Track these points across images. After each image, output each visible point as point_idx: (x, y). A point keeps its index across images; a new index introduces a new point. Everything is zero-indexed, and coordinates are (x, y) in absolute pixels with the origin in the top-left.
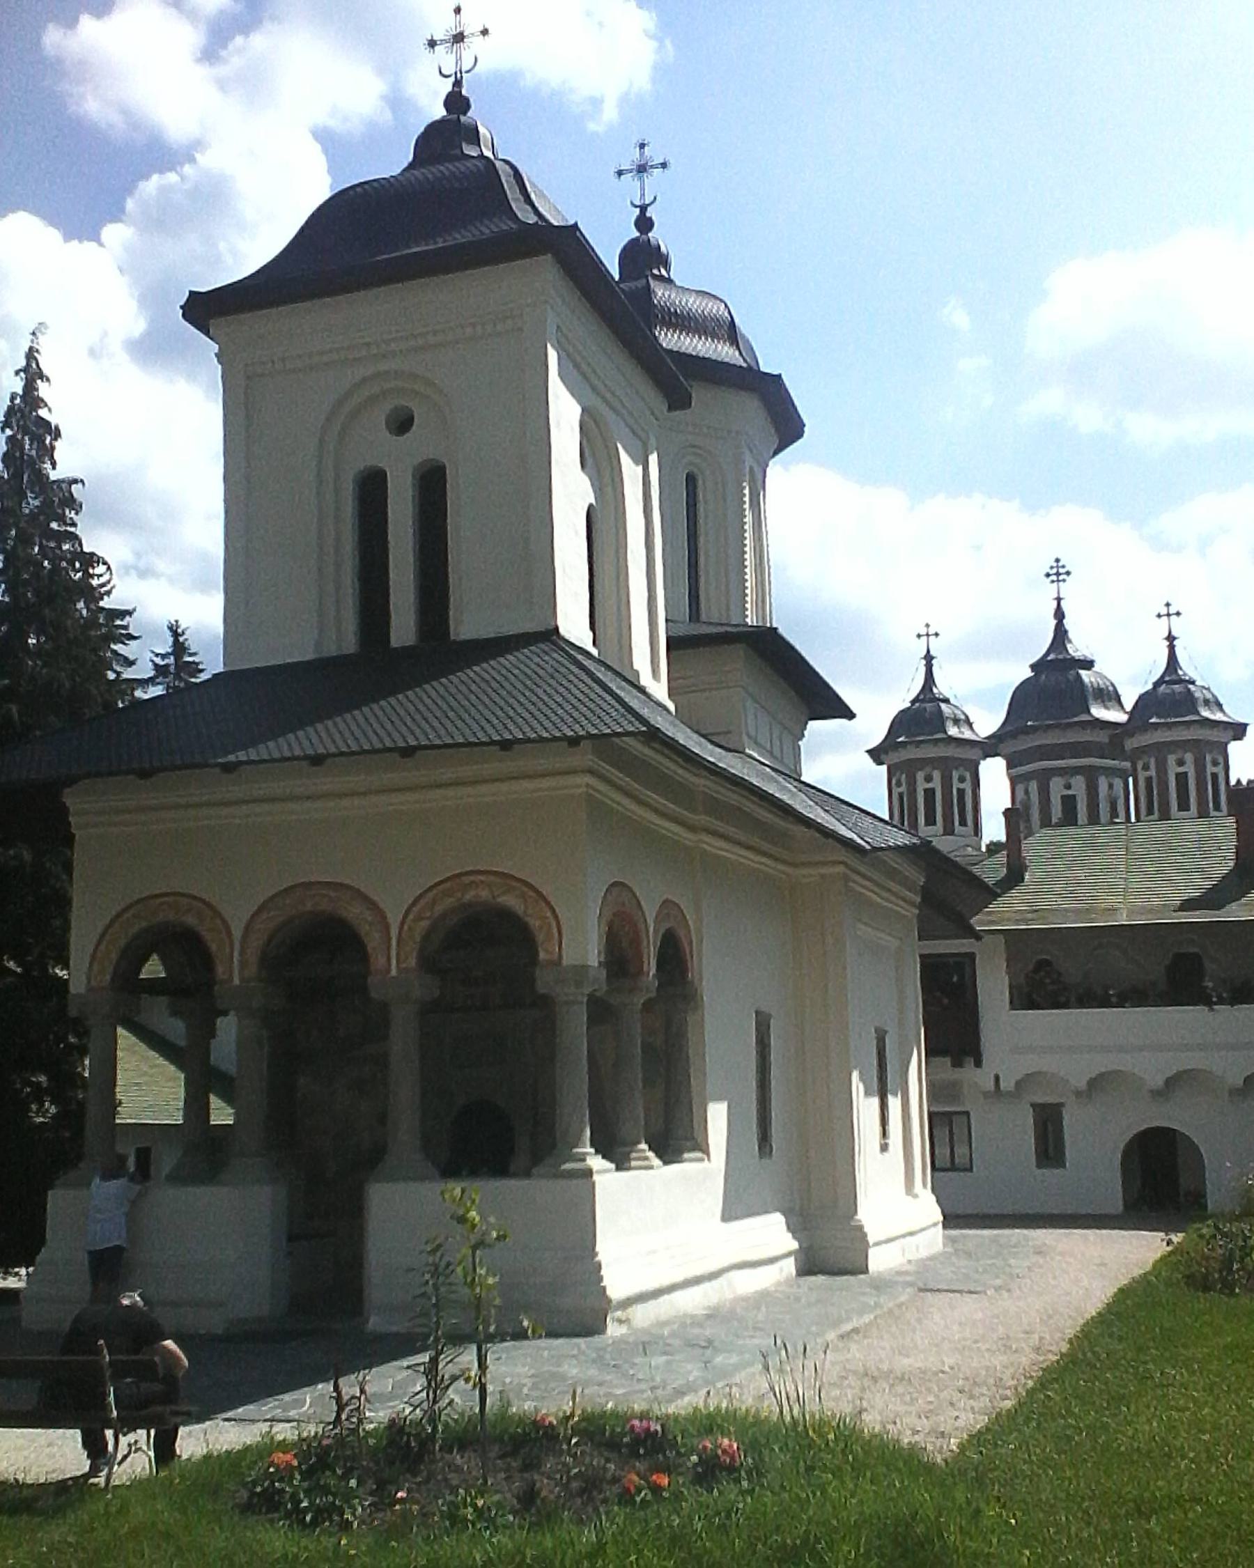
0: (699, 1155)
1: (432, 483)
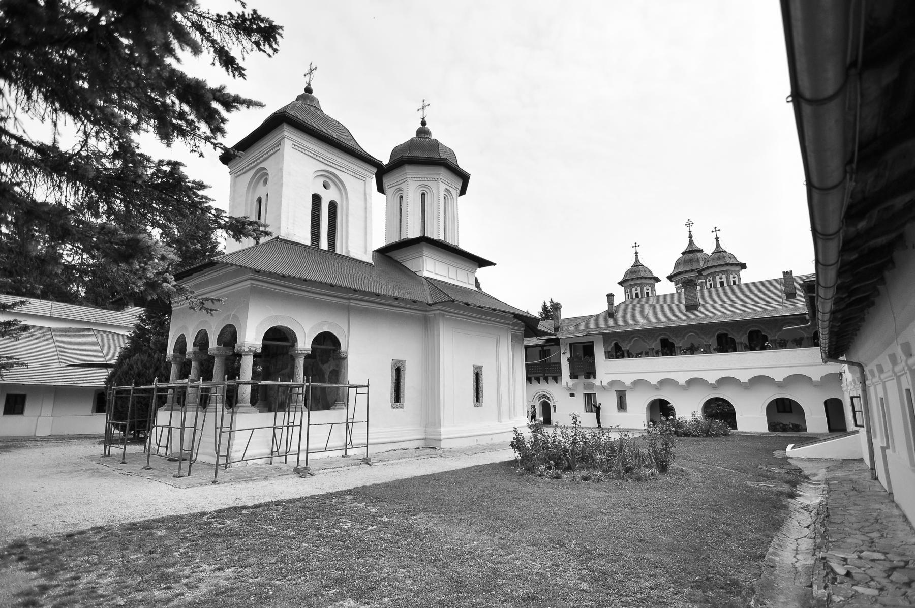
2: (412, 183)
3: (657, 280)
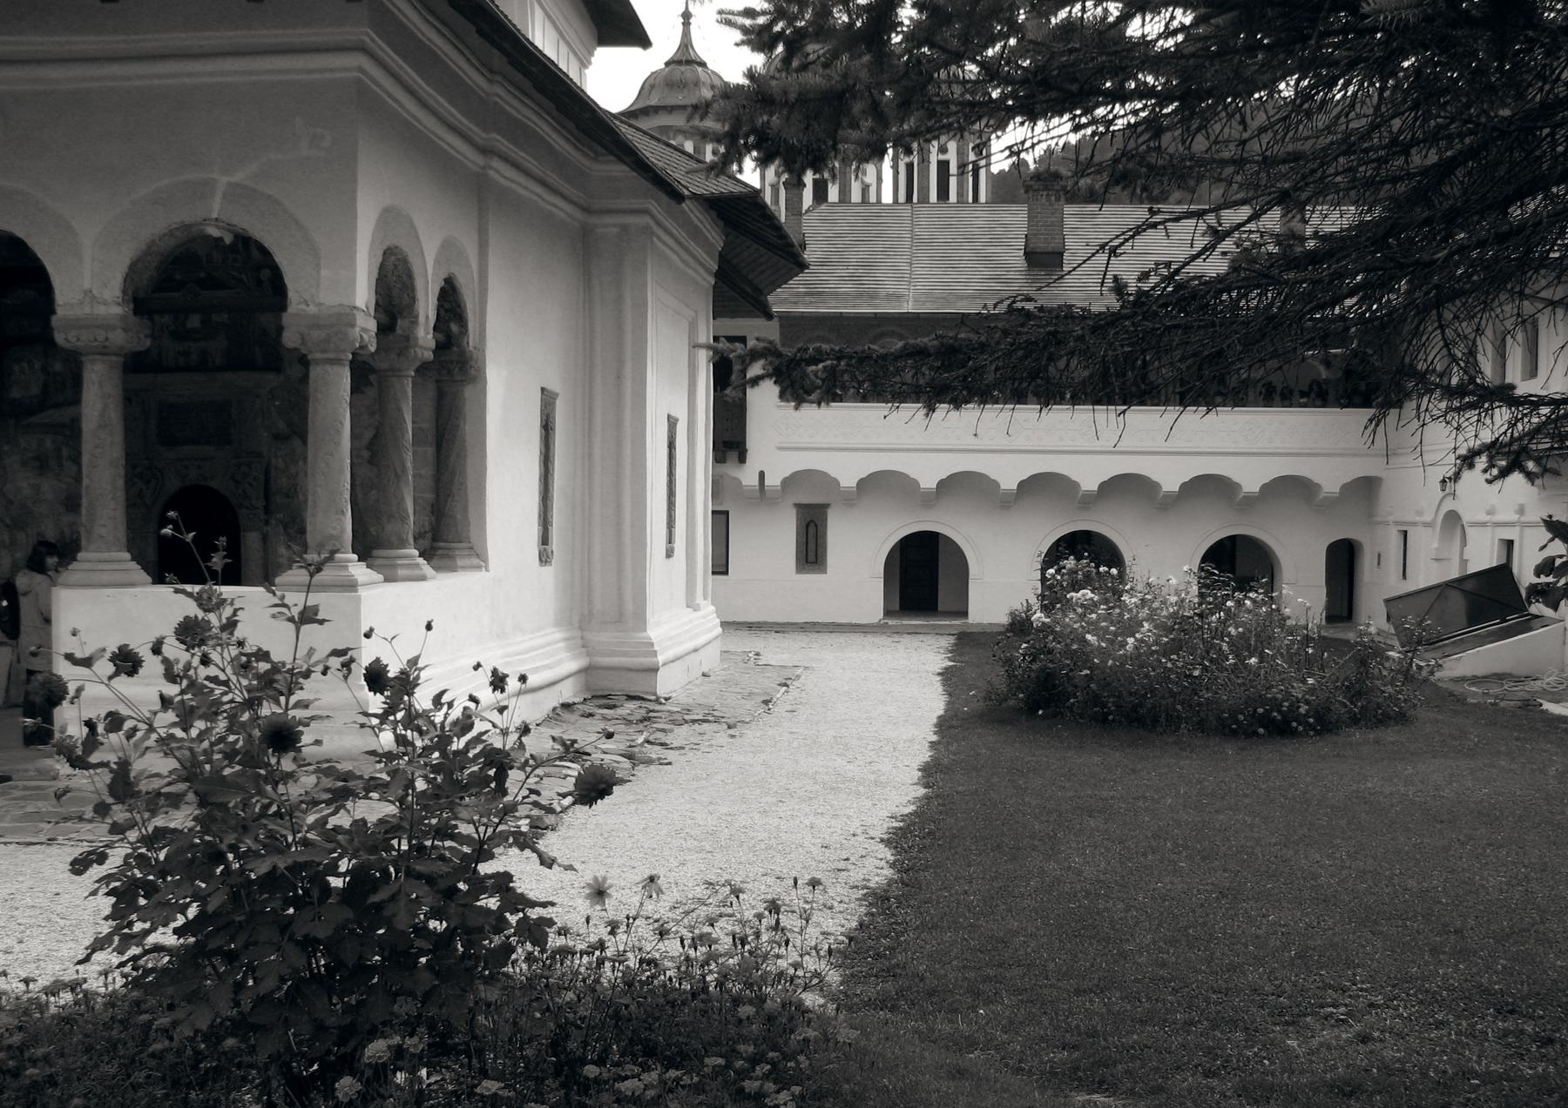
0: (476, 561)
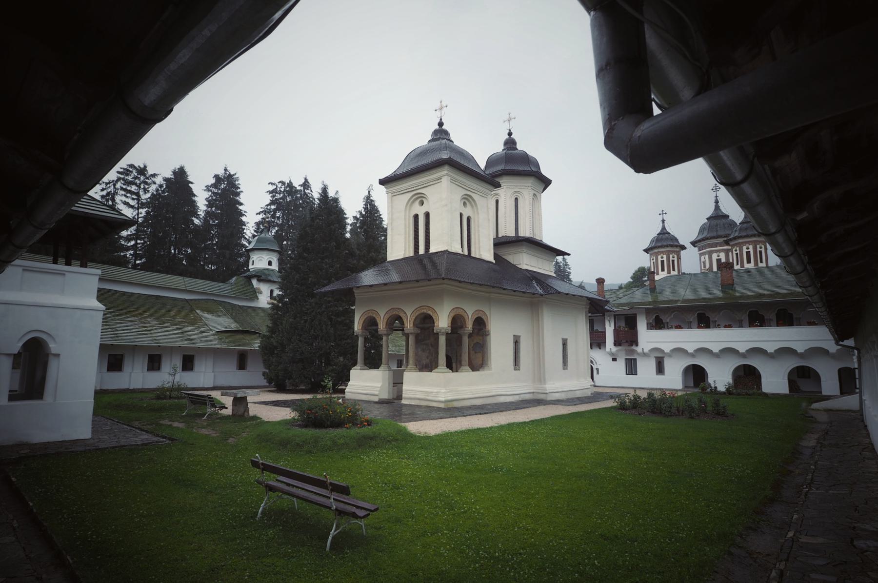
1: (427, 215)
2: (506, 192)
3: (683, 248)
